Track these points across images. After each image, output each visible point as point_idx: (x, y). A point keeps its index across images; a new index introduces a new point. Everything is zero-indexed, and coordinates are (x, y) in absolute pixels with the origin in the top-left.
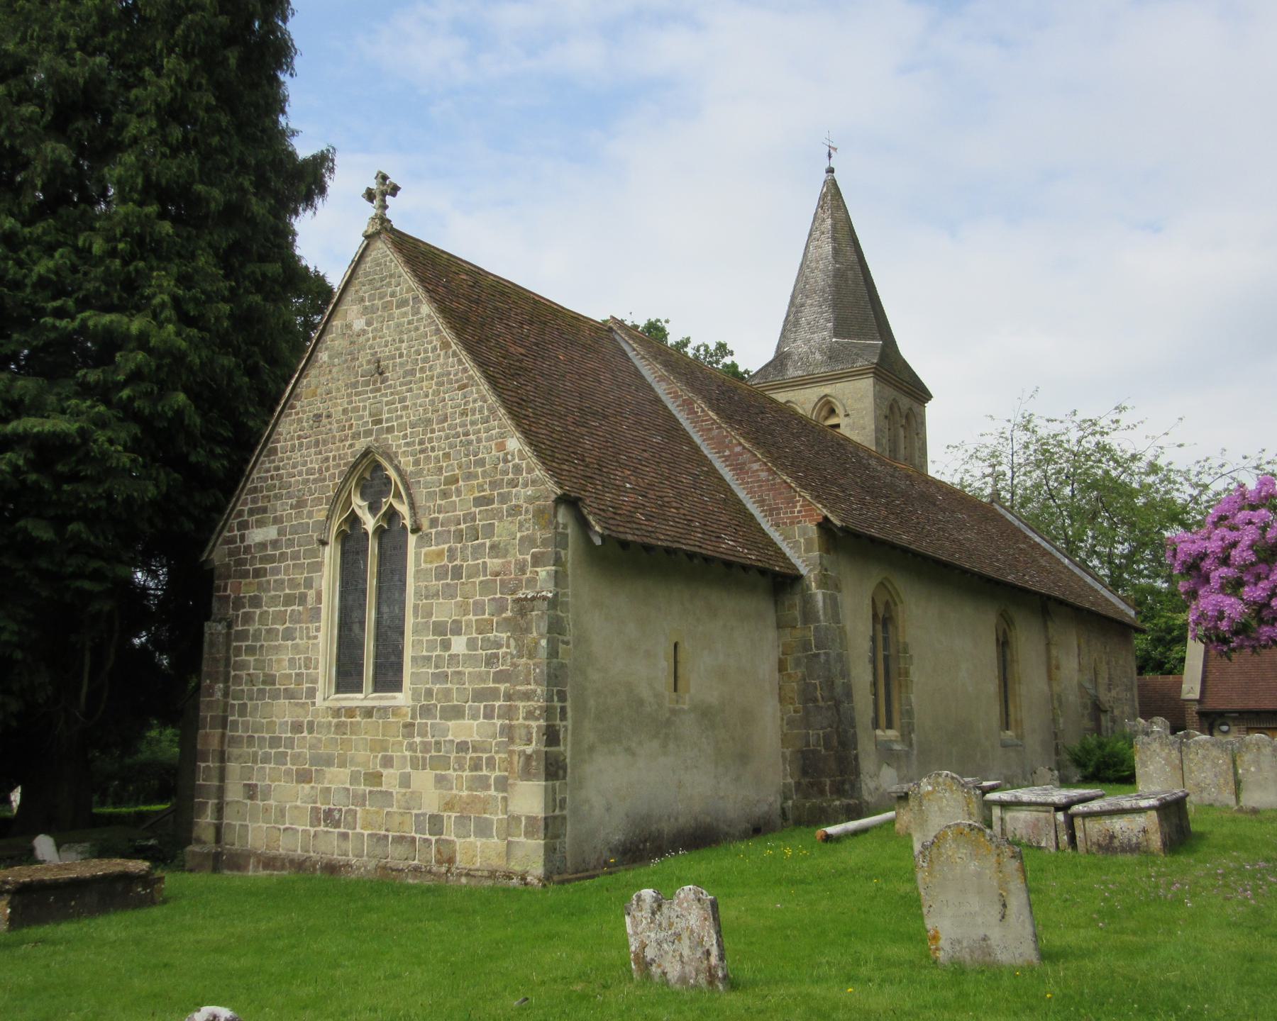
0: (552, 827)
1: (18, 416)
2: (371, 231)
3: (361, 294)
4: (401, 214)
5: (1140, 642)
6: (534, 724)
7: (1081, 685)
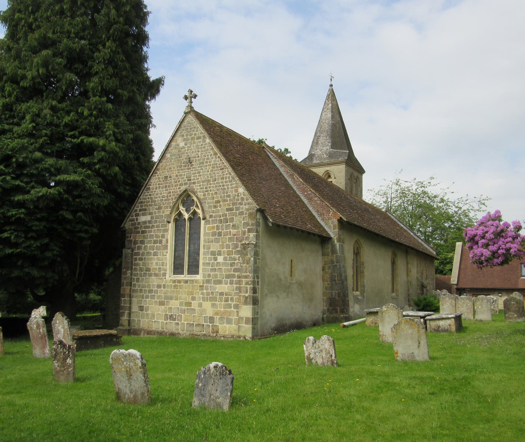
0: (254, 321)
1: (59, 174)
2: (187, 111)
3: (183, 133)
4: (198, 106)
5: (436, 263)
6: (249, 286)
7: (417, 278)
